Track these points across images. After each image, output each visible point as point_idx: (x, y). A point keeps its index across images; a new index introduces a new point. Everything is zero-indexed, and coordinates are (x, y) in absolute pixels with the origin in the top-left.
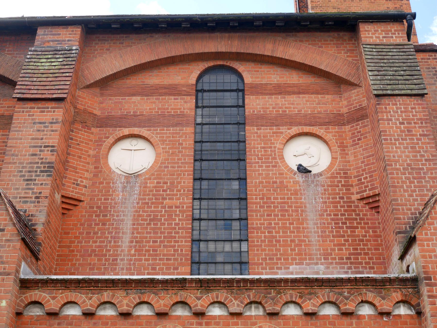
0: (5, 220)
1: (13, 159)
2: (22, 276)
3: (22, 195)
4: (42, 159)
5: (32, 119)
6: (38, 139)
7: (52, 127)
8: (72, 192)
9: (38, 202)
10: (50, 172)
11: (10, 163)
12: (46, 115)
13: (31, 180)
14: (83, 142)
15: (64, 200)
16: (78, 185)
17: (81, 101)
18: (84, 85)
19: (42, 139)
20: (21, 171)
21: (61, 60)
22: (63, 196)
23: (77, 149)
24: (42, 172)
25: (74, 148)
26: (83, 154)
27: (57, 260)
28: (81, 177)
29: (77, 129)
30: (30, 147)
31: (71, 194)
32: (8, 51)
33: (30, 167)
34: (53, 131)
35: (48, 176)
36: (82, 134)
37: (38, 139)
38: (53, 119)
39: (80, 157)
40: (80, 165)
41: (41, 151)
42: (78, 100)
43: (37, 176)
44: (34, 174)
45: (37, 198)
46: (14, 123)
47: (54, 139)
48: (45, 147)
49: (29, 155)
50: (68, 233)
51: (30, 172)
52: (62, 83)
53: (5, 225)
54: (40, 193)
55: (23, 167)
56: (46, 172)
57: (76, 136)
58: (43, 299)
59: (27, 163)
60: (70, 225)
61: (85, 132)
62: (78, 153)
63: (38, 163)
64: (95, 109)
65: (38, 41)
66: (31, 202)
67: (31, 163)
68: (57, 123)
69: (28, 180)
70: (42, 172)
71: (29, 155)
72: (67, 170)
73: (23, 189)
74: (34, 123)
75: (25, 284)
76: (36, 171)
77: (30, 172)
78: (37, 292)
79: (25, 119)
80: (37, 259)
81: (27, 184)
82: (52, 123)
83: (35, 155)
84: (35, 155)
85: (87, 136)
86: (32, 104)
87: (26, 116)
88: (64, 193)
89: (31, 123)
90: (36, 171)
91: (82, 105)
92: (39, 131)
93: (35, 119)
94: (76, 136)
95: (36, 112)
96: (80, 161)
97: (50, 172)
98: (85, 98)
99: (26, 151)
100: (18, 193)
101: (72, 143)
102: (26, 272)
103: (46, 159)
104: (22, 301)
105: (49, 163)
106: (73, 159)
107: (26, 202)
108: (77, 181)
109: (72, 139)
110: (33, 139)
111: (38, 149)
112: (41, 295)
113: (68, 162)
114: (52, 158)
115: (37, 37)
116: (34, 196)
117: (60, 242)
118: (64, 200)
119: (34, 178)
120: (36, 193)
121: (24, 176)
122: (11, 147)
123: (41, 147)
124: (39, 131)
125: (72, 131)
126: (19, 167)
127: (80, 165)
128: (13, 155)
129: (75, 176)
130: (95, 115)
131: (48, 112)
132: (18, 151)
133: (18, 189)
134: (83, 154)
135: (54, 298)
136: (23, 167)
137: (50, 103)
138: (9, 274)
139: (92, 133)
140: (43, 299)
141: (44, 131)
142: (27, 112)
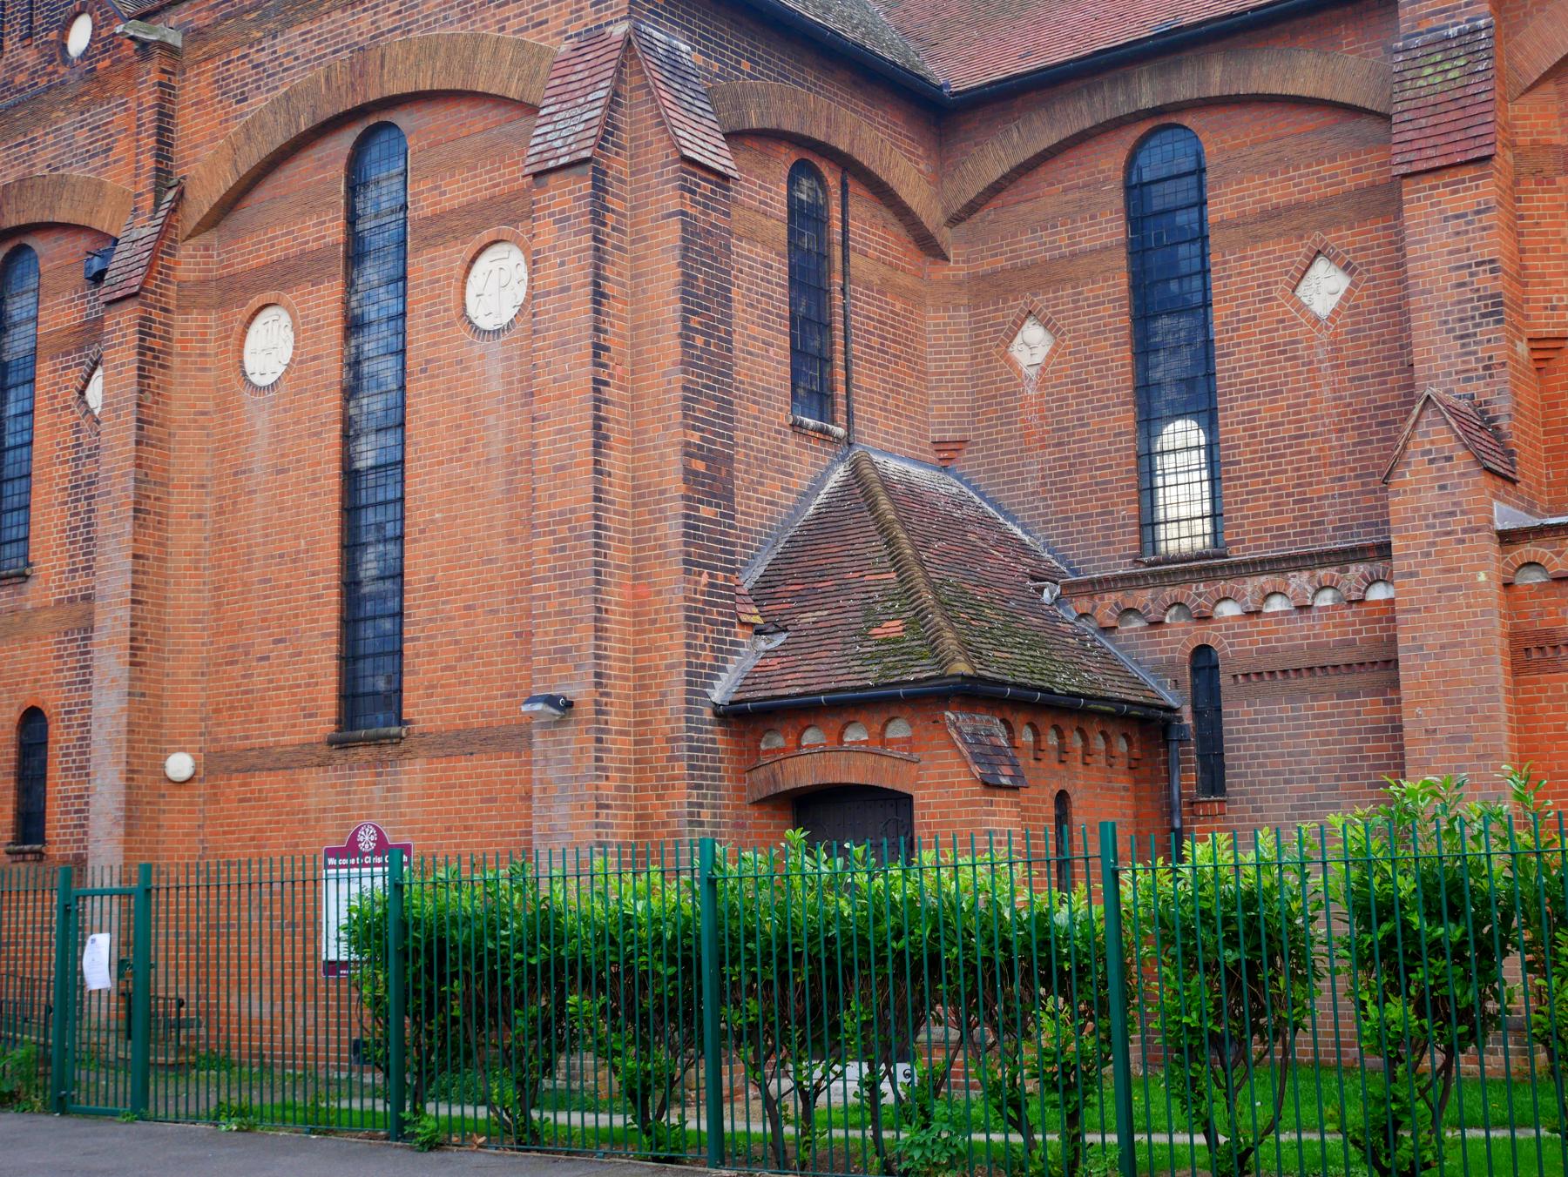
0: (1449, 440)
1: (1426, 301)
2: (1499, 526)
3: (1460, 368)
4: (1478, 290)
5: (1441, 212)
6: (1459, 251)
7: (1480, 221)
8: (1547, 325)
9: (1491, 376)
10: (1500, 313)
11: (1422, 309)
12: (1463, 199)
13: (1467, 336)
14: (1544, 216)
15: (1534, 345)
16: (1554, 308)
17: (1524, 126)
18: (1519, 90)
19: (1468, 250)
20: (1446, 322)
21: (1462, 62)
22: (1530, 340)
23: (1537, 234)
24: (1483, 316)
25: (1529, 234)
26: (1550, 242)
27: (1547, 459)
28: (1557, 291)
29: (1526, 191)
30: (1450, 270)
31: (1544, 332)
32: (1348, 44)
33: (1460, 311)
34: (1484, 229)
35: (1498, 322)
36: (1539, 200)
37: (1459, 251)
38: (1479, 204)
39: (1546, 250)
40: (1548, 267)
41: (1472, 275)
42: (1515, 126)
43: (1476, 326)
44: (1470, 323)
45: (1486, 368)
46: (1408, 228)
47: (1493, 245)
48: (1478, 264)
49: (1453, 287)
50: (1556, 405)
51: (1461, 320)
52: (1479, 120)
53: (1452, 449)
54: (1490, 358)
55: (1447, 314)
56: (1491, 314)
57: (1528, 209)
58: (1542, 558)
59: (1452, 304)
60: (1555, 389)
61: (1545, 191)
62: (1539, 242)
63: (1472, 300)
64: (1554, 133)
65: (1405, 21)
66: (1478, 378)
67: (1459, 302)
68: (1488, 209)
69: (1462, 337)
70: (1483, 316)
71: (1453, 287)
72: (1526, 284)
73: (1459, 355)
74: (1446, 219)
75: (1507, 538)
76: (1473, 318)
77: (1461, 320)
78: (1528, 546)
79: (1427, 215)
80: (1514, 482)
81: (1463, 345)
82: (1478, 212)
83: (1463, 284)
84: (1463, 284)
85: (1550, 199)
86: (1432, 180)
87: (1425, 207)
88: (1531, 332)
89: (1439, 221)
90: (1473, 318)
91: (1524, 134)
92: (1458, 233)
93: (1444, 211)
94: (1528, 209)
95: (1443, 194)
96: (1549, 259)
97: (1500, 313)
98: (1526, 118)
99: (1445, 280)
100: (1451, 365)
101: (1523, 226)
102: (1506, 516)
103: (1485, 289)
104: (1508, 564)
105: (1492, 296)
106: (1534, 259)
107: (1469, 379)
108: (1550, 300)
109: (1521, 217)
110: (1450, 253)
111: (1467, 271)
112: (1536, 553)
113: (1524, 268)
114: (1498, 285)
115: (1401, 12)
116: (1480, 365)
117: (1544, 425)
118: (1534, 345)
119: (1471, 331)
120: (1483, 359)
121: (1453, 330)
122: (1415, 276)
123: (1470, 266)
124: (1458, 233)
125: (1519, 200)
126: (1439, 314)
127: (1548, 267)
128: (1423, 292)
129: (1544, 292)
130: (1559, 146)
131: (1466, 189)
132: (1431, 283)
133: (1448, 357)
134: (1550, 242)
135: (1559, 554)
136: (1447, 314)
137: (1464, 169)
138: (1478, 530)
139: (1559, 190)
140: (1542, 558)
141: (1467, 232)
142: (1426, 198)
